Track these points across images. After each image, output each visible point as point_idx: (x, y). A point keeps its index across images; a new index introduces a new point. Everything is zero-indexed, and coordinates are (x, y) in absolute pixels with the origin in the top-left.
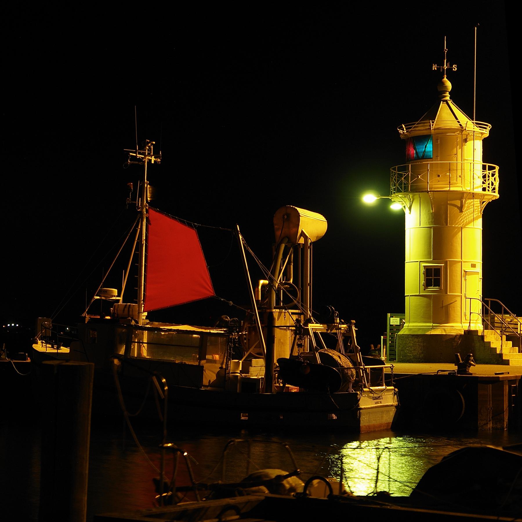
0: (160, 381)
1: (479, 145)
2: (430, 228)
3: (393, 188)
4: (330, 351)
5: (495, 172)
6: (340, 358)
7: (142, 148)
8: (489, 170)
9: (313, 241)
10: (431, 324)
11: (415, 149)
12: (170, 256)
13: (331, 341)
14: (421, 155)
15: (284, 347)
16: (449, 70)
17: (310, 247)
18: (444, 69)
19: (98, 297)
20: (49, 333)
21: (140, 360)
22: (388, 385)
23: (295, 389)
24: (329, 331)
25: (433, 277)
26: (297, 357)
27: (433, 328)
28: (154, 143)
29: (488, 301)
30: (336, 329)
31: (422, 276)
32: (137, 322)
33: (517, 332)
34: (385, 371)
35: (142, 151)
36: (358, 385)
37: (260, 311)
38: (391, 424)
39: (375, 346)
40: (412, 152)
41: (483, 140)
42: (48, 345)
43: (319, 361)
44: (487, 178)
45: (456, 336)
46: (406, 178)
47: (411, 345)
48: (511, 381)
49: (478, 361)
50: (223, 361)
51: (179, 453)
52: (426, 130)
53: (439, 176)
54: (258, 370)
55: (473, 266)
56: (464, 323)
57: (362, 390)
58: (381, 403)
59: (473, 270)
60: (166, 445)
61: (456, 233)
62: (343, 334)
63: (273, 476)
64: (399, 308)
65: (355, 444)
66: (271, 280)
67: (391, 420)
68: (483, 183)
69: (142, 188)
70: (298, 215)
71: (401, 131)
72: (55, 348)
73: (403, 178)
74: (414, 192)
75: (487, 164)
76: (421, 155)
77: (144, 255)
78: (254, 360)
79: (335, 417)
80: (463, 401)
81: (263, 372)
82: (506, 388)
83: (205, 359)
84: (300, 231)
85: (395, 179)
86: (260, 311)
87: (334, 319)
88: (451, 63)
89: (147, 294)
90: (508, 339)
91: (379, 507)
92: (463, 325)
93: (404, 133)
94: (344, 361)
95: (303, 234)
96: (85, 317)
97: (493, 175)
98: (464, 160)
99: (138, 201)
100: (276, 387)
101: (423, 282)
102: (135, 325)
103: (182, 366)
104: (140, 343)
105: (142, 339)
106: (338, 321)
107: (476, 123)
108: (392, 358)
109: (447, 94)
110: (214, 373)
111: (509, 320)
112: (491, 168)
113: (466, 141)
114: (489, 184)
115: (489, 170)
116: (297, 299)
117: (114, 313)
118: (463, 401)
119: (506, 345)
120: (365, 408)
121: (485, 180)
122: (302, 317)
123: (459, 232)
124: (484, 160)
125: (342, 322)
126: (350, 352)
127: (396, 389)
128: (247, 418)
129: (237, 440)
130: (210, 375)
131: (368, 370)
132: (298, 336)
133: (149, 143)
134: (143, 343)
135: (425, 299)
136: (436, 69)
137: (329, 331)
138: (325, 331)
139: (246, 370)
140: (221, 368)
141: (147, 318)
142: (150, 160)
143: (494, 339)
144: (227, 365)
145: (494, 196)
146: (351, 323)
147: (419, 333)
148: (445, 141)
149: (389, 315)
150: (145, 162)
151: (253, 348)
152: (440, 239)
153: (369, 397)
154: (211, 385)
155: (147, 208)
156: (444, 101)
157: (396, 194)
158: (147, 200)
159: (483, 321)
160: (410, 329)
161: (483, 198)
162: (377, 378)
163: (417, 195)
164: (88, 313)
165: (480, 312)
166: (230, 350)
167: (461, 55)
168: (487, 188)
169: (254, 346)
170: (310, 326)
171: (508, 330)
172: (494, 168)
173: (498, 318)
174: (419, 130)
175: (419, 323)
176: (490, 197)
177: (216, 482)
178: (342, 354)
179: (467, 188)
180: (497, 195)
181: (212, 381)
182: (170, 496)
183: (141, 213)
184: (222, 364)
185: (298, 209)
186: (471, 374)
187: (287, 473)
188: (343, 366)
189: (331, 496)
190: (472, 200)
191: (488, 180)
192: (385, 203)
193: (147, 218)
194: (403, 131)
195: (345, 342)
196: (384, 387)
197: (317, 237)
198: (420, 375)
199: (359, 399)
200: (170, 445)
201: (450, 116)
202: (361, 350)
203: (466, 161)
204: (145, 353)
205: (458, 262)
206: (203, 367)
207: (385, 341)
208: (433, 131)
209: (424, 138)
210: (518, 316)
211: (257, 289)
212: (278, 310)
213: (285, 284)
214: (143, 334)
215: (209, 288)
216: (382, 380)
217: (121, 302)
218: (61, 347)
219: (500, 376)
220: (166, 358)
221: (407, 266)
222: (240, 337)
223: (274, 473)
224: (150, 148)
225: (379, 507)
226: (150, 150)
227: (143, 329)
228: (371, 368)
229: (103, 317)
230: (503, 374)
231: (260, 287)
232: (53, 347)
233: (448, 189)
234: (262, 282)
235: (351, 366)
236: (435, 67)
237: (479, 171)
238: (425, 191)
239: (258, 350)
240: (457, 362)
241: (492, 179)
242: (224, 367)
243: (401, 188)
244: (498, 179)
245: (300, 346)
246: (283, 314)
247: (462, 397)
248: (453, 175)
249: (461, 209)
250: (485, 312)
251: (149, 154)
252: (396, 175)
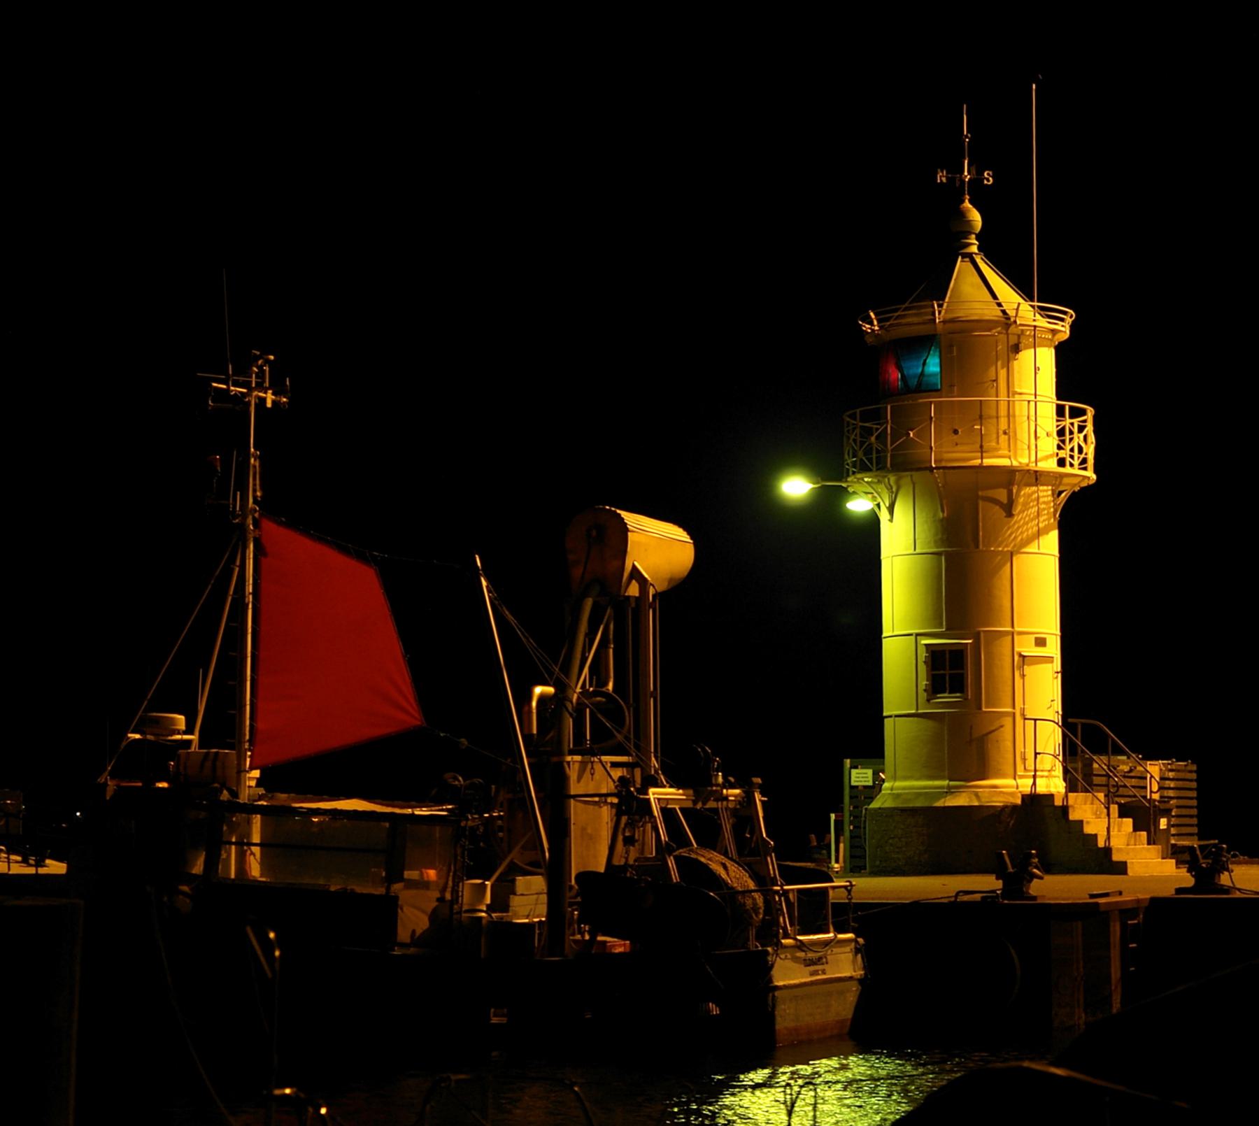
1: (1047, 358)
5: (1085, 421)
8: (1071, 417)
9: (659, 589)
10: (945, 783)
11: (900, 369)
12: (317, 635)
13: (706, 827)
15: (593, 844)
16: (977, 182)
19: (138, 736)
21: (244, 884)
23: (620, 946)
24: (699, 806)
25: (954, 670)
27: (950, 791)
28: (272, 357)
29: (1075, 724)
30: (717, 800)
31: (923, 668)
32: (235, 794)
33: (1145, 797)
36: (770, 933)
40: (894, 375)
41: (1057, 348)
42: (13, 857)
43: (675, 876)
44: (1068, 437)
46: (881, 438)
48: (1126, 912)
49: (1049, 868)
50: (447, 883)
51: (311, 1110)
52: (924, 323)
54: (530, 902)
56: (1021, 777)
57: (778, 945)
58: (824, 972)
59: (1040, 652)
60: (277, 1092)
61: (1000, 566)
62: (734, 813)
65: (759, 1075)
66: (561, 687)
67: (850, 1016)
68: (1059, 448)
70: (624, 529)
72: (32, 862)
73: (873, 439)
75: (1068, 404)
78: (521, 881)
79: (715, 1010)
80: (1016, 960)
81: (543, 909)
82: (1116, 929)
83: (400, 879)
84: (628, 567)
85: (855, 440)
87: (710, 777)
88: (978, 167)
89: (260, 725)
90: (1122, 814)
92: (1020, 781)
93: (873, 331)
94: (736, 876)
95: (635, 573)
96: (106, 784)
97: (1081, 429)
98: (1016, 393)
99: (235, 500)
100: (575, 941)
101: (923, 683)
102: (229, 801)
103: (347, 896)
104: (243, 844)
105: (249, 835)
106: (720, 780)
107: (1039, 307)
108: (856, 867)
109: (973, 240)
110: (424, 912)
111: (1126, 768)
112: (1075, 413)
113: (1016, 349)
114: (1072, 450)
115: (1071, 417)
118: (1016, 960)
119: (1120, 826)
120: (785, 987)
121: (1063, 442)
122: (638, 772)
123: (1005, 564)
124: (1059, 396)
125: (729, 782)
126: (749, 854)
127: (861, 940)
128: (504, 1020)
129: (453, 1077)
130: (414, 918)
131: (791, 896)
132: (624, 819)
133: (260, 357)
134: (250, 844)
135: (929, 724)
136: (944, 180)
137: (699, 806)
138: (689, 805)
139: (501, 902)
140: (441, 900)
141: (260, 783)
142: (264, 400)
143: (1090, 813)
144: (455, 892)
145: (1084, 477)
146: (751, 785)
147: (919, 803)
148: (977, 351)
149: (848, 761)
151: (517, 849)
152: (963, 579)
153: (795, 959)
154: (416, 941)
155: (257, 515)
156: (965, 256)
157: (859, 476)
158: (255, 497)
159: (1066, 772)
160: (898, 796)
161: (1060, 484)
162: (814, 913)
163: (906, 479)
164: (113, 775)
167: (998, 146)
168: (1068, 459)
170: (653, 793)
172: (1083, 412)
173: (1099, 764)
176: (1076, 480)
178: (731, 859)
179: (1022, 459)
180: (1091, 475)
181: (418, 932)
183: (242, 528)
185: (624, 514)
186: (1035, 898)
188: (733, 888)
190: (1034, 488)
191: (1071, 440)
192: (829, 499)
193: (256, 542)
194: (872, 326)
195: (738, 830)
196: (831, 935)
197: (671, 580)
199: (772, 966)
200: (288, 1091)
201: (982, 290)
203: (1017, 397)
204: (255, 870)
205: (1006, 633)
206: (396, 898)
207: (839, 824)
208: (940, 327)
211: (526, 708)
212: (578, 758)
213: (595, 694)
214: (249, 822)
215: (411, 710)
216: (826, 918)
218: (48, 861)
219: (1102, 901)
220: (307, 880)
221: (886, 644)
226: (261, 375)
227: (251, 809)
228: (799, 890)
230: (1106, 895)
231: (534, 704)
232: (25, 861)
233: (977, 462)
234: (538, 690)
236: (941, 177)
240: (1000, 873)
241: (1078, 438)
242: (448, 896)
243: (870, 460)
244: (1092, 438)
245: (629, 841)
248: (988, 429)
249: (1009, 508)
250: (1069, 750)
251: (260, 386)
252: (858, 431)
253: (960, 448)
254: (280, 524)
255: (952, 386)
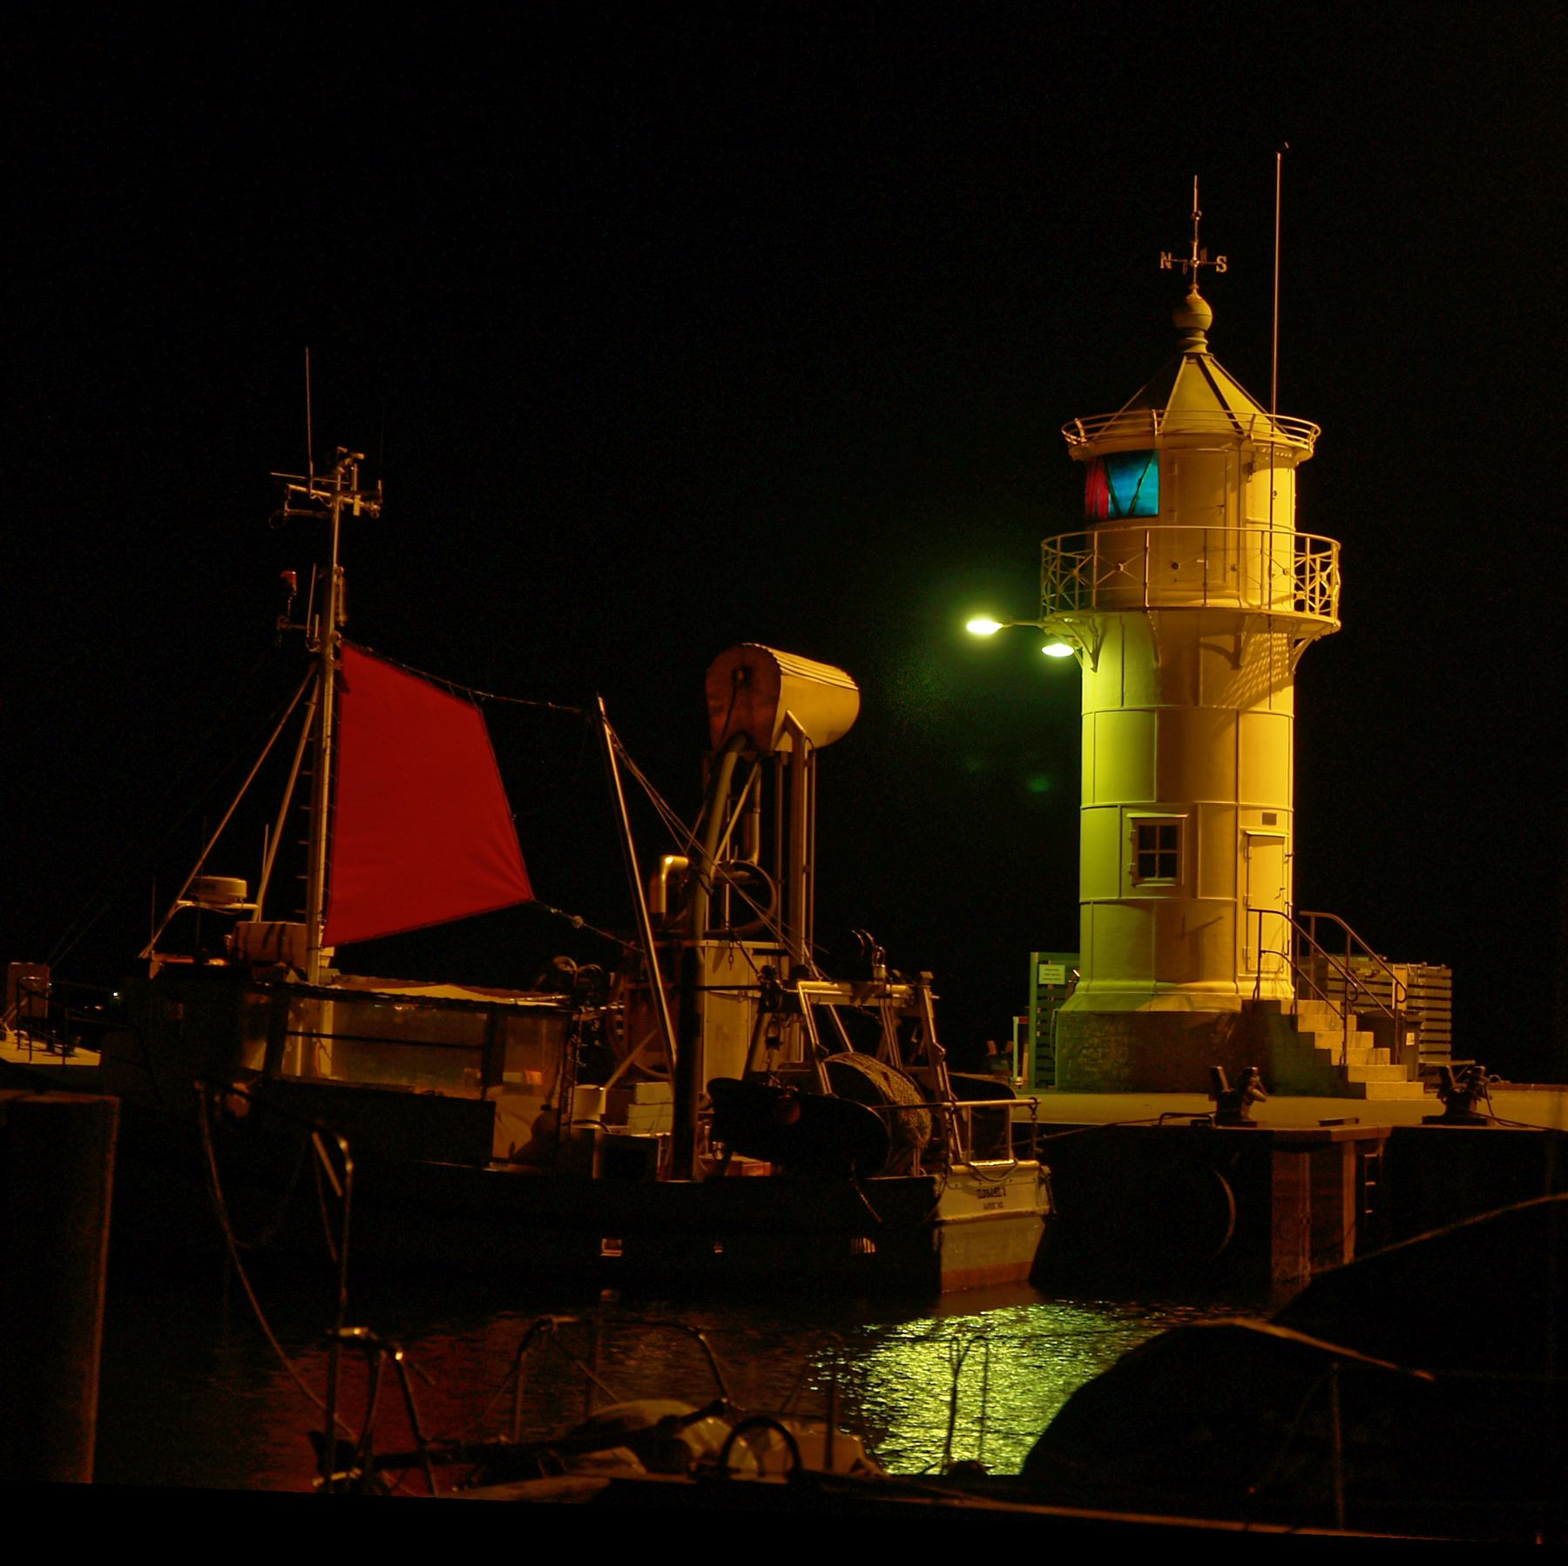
0: (332, 1147)
1: (1285, 480)
2: (1151, 711)
3: (1047, 596)
4: (860, 1058)
5: (1329, 557)
6: (886, 1078)
7: (326, 469)
10: (1151, 983)
14: (1126, 506)
15: (729, 1045)
16: (1207, 271)
17: (808, 763)
18: (1191, 269)
19: (189, 903)
20: (42, 1008)
21: (312, 1088)
22: (1021, 1155)
24: (857, 1004)
25: (1158, 849)
26: (765, 1076)
27: (1156, 994)
28: (361, 456)
29: (1308, 919)
30: (878, 997)
31: (1128, 847)
32: (303, 976)
33: (1389, 1007)
34: (1015, 1116)
35: (324, 481)
36: (936, 1156)
37: (660, 944)
38: (1028, 1268)
39: (1000, 1047)
41: (1297, 469)
42: (36, 1044)
43: (827, 1088)
44: (1308, 575)
45: (1221, 1015)
47: (1096, 1041)
48: (1364, 1144)
50: (554, 1088)
51: (384, 1354)
53: (1175, 566)
54: (652, 1114)
55: (1270, 819)
56: (1242, 979)
57: (947, 1171)
58: (1001, 1205)
60: (344, 1332)
62: (899, 1013)
63: (654, 1420)
64: (1065, 940)
65: (921, 1327)
66: (696, 857)
68: (1298, 588)
69: (324, 585)
70: (776, 672)
71: (1071, 439)
72: (58, 1051)
73: (1076, 572)
74: (1105, 610)
75: (1309, 536)
76: (1126, 506)
77: (326, 781)
78: (642, 1088)
79: (869, 1247)
83: (499, 1081)
86: (660, 944)
87: (871, 969)
90: (1362, 1026)
91: (927, 1501)
94: (899, 1089)
95: (788, 724)
96: (149, 960)
97: (1324, 566)
99: (313, 624)
100: (706, 1162)
101: (1129, 863)
103: (433, 1101)
104: (312, 1035)
105: (319, 1024)
106: (883, 973)
108: (1043, 1080)
110: (526, 1121)
111: (1368, 972)
112: (1318, 547)
113: (1250, 469)
114: (1313, 591)
116: (771, 912)
117: (235, 949)
119: (1358, 1041)
120: (954, 1222)
121: (1303, 581)
122: (785, 961)
123: (1229, 724)
126: (914, 1060)
127: (1046, 1169)
128: (618, 1253)
129: (556, 1320)
130: (513, 1130)
131: (964, 1114)
133: (347, 455)
135: (1135, 913)
136: (1169, 265)
138: (845, 1002)
139: (617, 1114)
140: (546, 1108)
141: (334, 963)
142: (350, 507)
143: (1324, 1026)
144: (563, 1099)
146: (920, 979)
149: (1035, 956)
150: (332, 511)
152: (1179, 739)
153: (967, 1190)
154: (514, 1158)
155: (338, 644)
156: (1190, 356)
157: (1058, 615)
159: (1295, 973)
160: (1093, 999)
161: (1298, 631)
162: (990, 1135)
164: (159, 949)
165: (1288, 949)
166: (574, 1057)
169: (646, 1041)
170: (803, 987)
171: (1361, 999)
172: (1328, 547)
173: (1336, 965)
174: (1123, 437)
175: (1118, 978)
176: (1316, 627)
177: (493, 1440)
178: (894, 1068)
180: (1334, 621)
182: (354, 1483)
183: (320, 658)
184: (550, 1096)
185: (777, 654)
186: (1254, 1124)
187: (695, 1410)
189: (796, 1472)
191: (1312, 579)
193: (338, 675)
195: (902, 1035)
197: (830, 734)
198: (1111, 1128)
199: (940, 1196)
200: (357, 1331)
201: (1210, 397)
202: (946, 1058)
203: (1249, 527)
205: (1230, 806)
206: (493, 1104)
207: (1023, 1030)
208: (1159, 441)
209: (1134, 458)
210: (1392, 960)
211: (653, 883)
212: (714, 943)
213: (738, 867)
214: (319, 1009)
216: (1004, 1142)
217: (257, 918)
218: (78, 1050)
222: (605, 1017)
223: (656, 1409)
224: (349, 472)
225: (927, 1501)
226: (347, 476)
227: (322, 994)
228: (974, 1108)
229: (201, 960)
230: (1340, 1122)
232: (50, 1049)
235: (917, 1099)
236: (1166, 261)
237: (1285, 555)
238: (1138, 609)
239: (655, 1057)
240: (1214, 1090)
241: (1320, 578)
242: (555, 1104)
243: (1072, 597)
244: (1337, 577)
245: (773, 1043)
246: (728, 953)
247: (1228, 1191)
249: (1235, 659)
250: (1300, 948)
252: (1058, 562)
253: (1178, 585)
254: (366, 654)
255: (1171, 511)
